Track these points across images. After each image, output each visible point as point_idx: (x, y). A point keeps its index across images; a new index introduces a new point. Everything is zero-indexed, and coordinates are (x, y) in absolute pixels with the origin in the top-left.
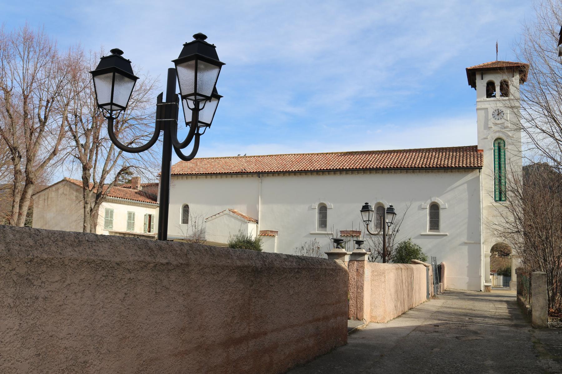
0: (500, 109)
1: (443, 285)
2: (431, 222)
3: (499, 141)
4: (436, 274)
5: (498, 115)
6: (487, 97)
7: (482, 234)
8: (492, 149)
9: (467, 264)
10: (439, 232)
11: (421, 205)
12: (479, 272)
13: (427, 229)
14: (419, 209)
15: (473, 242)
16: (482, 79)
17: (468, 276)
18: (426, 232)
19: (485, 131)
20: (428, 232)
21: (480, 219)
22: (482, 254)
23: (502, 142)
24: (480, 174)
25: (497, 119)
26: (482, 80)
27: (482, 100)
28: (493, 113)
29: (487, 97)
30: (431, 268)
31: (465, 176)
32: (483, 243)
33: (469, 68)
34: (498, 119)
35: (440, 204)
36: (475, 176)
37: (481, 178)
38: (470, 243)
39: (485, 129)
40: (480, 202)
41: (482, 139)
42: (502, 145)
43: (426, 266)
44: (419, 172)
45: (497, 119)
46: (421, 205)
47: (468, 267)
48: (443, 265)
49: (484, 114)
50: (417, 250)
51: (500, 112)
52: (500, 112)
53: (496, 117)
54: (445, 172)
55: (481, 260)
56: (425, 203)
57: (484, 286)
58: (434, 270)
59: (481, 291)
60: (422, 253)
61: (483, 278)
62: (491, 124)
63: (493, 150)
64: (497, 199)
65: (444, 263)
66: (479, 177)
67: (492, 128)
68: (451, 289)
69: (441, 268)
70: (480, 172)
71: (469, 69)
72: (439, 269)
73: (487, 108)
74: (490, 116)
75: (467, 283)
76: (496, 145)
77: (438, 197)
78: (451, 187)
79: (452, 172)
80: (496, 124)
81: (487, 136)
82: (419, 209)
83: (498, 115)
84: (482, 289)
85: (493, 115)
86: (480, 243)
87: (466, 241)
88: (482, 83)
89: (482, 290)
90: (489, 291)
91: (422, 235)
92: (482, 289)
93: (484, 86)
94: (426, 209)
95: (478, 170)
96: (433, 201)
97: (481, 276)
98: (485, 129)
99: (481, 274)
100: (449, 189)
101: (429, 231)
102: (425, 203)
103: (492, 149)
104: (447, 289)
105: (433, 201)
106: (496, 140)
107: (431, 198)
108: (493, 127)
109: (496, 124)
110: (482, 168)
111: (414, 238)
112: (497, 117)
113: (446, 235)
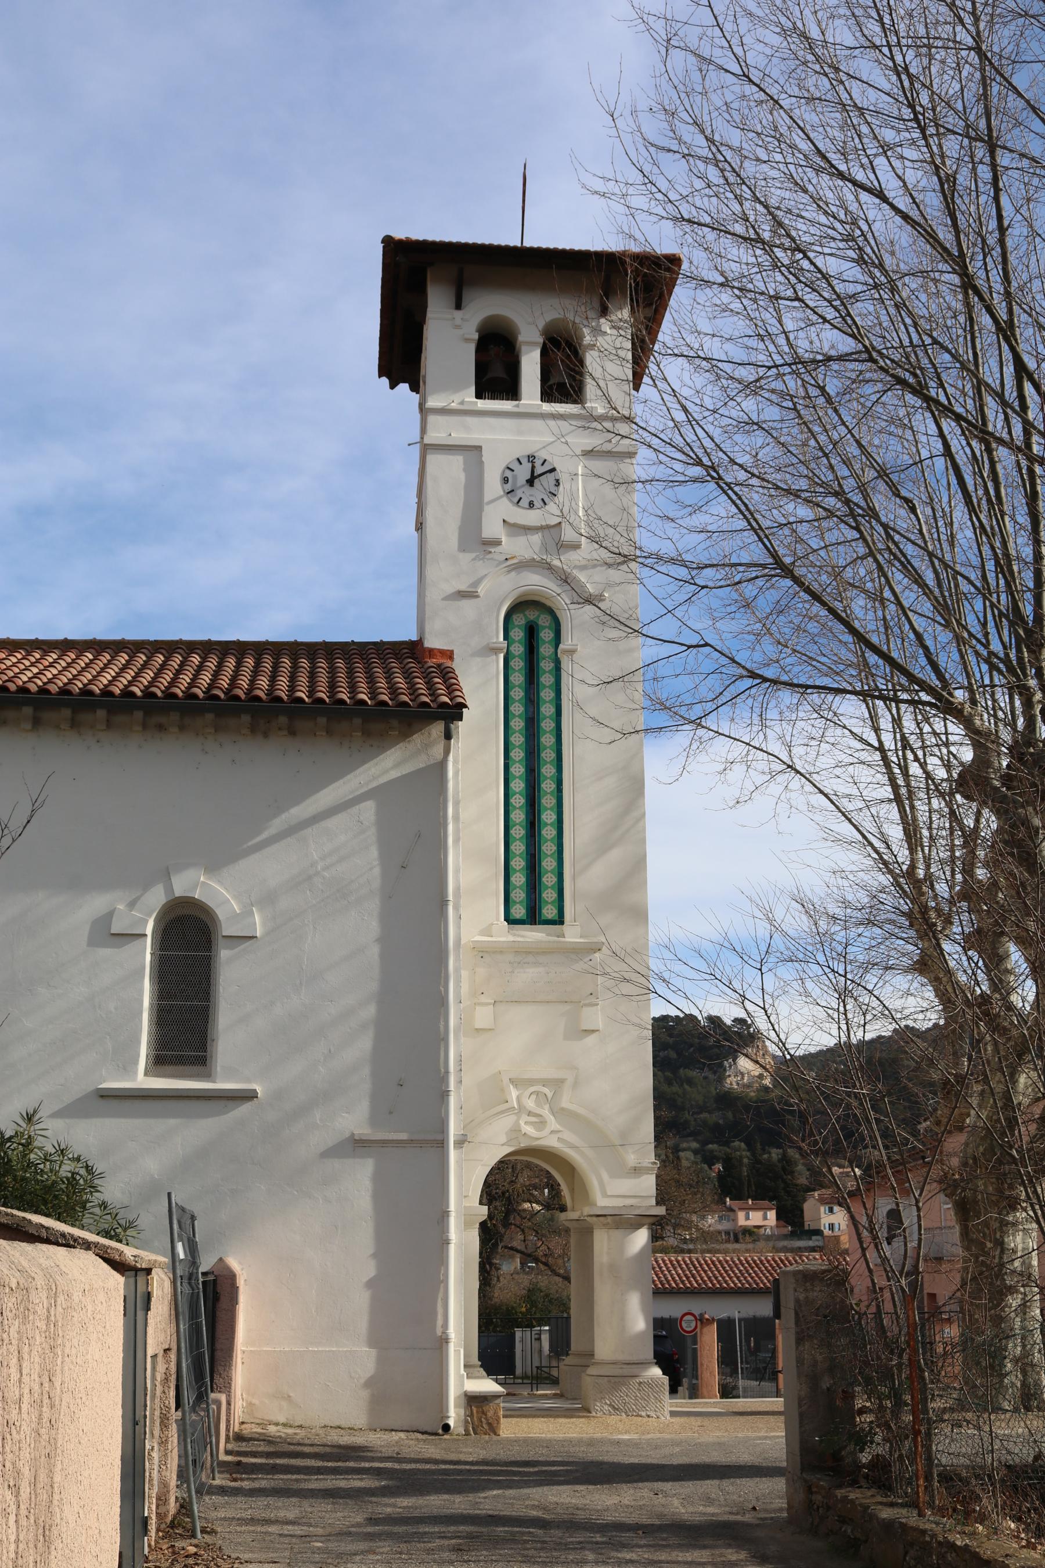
0: (543, 455)
1: (229, 1403)
2: (163, 1016)
3: (532, 615)
4: (195, 1330)
5: (531, 482)
6: (479, 395)
7: (452, 1086)
8: (500, 650)
9: (370, 1270)
10: (208, 1076)
11: (110, 915)
12: (434, 1313)
13: (136, 1062)
14: (94, 941)
15: (404, 1136)
16: (458, 306)
17: (374, 1340)
18: (134, 1079)
19: (466, 558)
20: (142, 1080)
21: (443, 1002)
22: (452, 1207)
23: (544, 620)
24: (447, 751)
25: (525, 503)
26: (458, 314)
27: (454, 405)
28: (508, 474)
29: (479, 395)
30: (161, 1286)
31: (364, 762)
32: (460, 1143)
33: (399, 234)
34: (531, 505)
35: (221, 914)
36: (420, 763)
37: (450, 773)
38: (384, 1143)
39: (463, 548)
40: (444, 903)
41: (447, 598)
42: (546, 635)
43: (119, 1266)
44: (109, 725)
45: (525, 503)
46: (110, 915)
47: (370, 1284)
48: (232, 1277)
49: (462, 477)
50: (72, 1180)
51: (539, 470)
52: (539, 470)
53: (519, 493)
54: (253, 730)
55: (447, 1242)
56: (132, 905)
57: (463, 1401)
58: (184, 1308)
59: (446, 1428)
60: (103, 1205)
61: (457, 1352)
62: (492, 527)
63: (501, 656)
64: (519, 911)
65: (234, 1263)
66: (442, 765)
67: (497, 543)
68: (272, 1429)
69: (216, 1298)
70: (448, 736)
71: (400, 242)
72: (210, 1304)
73: (479, 448)
74: (493, 486)
75: (369, 1383)
76: (518, 634)
77: (212, 869)
78: (283, 816)
79: (292, 733)
80: (514, 528)
81: (477, 583)
82: (94, 941)
83: (531, 482)
84: (454, 1416)
85: (506, 480)
86: (441, 1144)
87: (364, 1131)
88: (458, 327)
89: (451, 1422)
90: (493, 1429)
91: (106, 1095)
92: (454, 1416)
93: (467, 340)
94: (138, 942)
95: (437, 729)
96: (180, 889)
97: (445, 1340)
98: (463, 548)
99: (446, 1325)
100: (277, 824)
101: (146, 1073)
102: (132, 905)
103: (495, 651)
104: (248, 1430)
105: (178, 893)
106: (519, 607)
107: (166, 876)
108: (504, 539)
109: (514, 528)
110: (460, 718)
111: (57, 1115)
112: (527, 494)
113: (249, 1096)
